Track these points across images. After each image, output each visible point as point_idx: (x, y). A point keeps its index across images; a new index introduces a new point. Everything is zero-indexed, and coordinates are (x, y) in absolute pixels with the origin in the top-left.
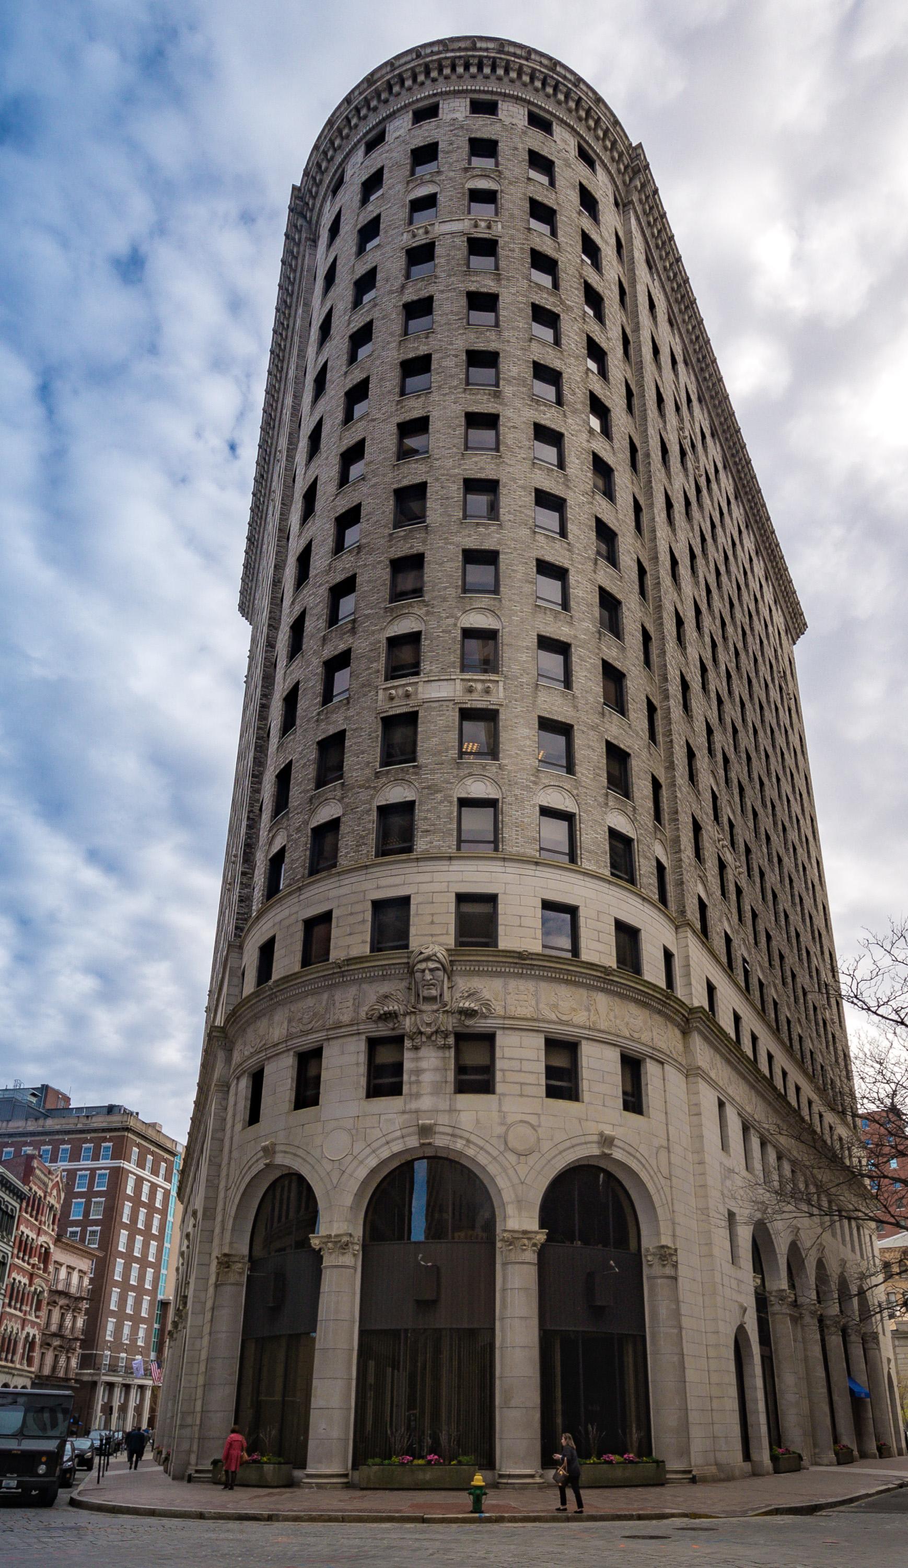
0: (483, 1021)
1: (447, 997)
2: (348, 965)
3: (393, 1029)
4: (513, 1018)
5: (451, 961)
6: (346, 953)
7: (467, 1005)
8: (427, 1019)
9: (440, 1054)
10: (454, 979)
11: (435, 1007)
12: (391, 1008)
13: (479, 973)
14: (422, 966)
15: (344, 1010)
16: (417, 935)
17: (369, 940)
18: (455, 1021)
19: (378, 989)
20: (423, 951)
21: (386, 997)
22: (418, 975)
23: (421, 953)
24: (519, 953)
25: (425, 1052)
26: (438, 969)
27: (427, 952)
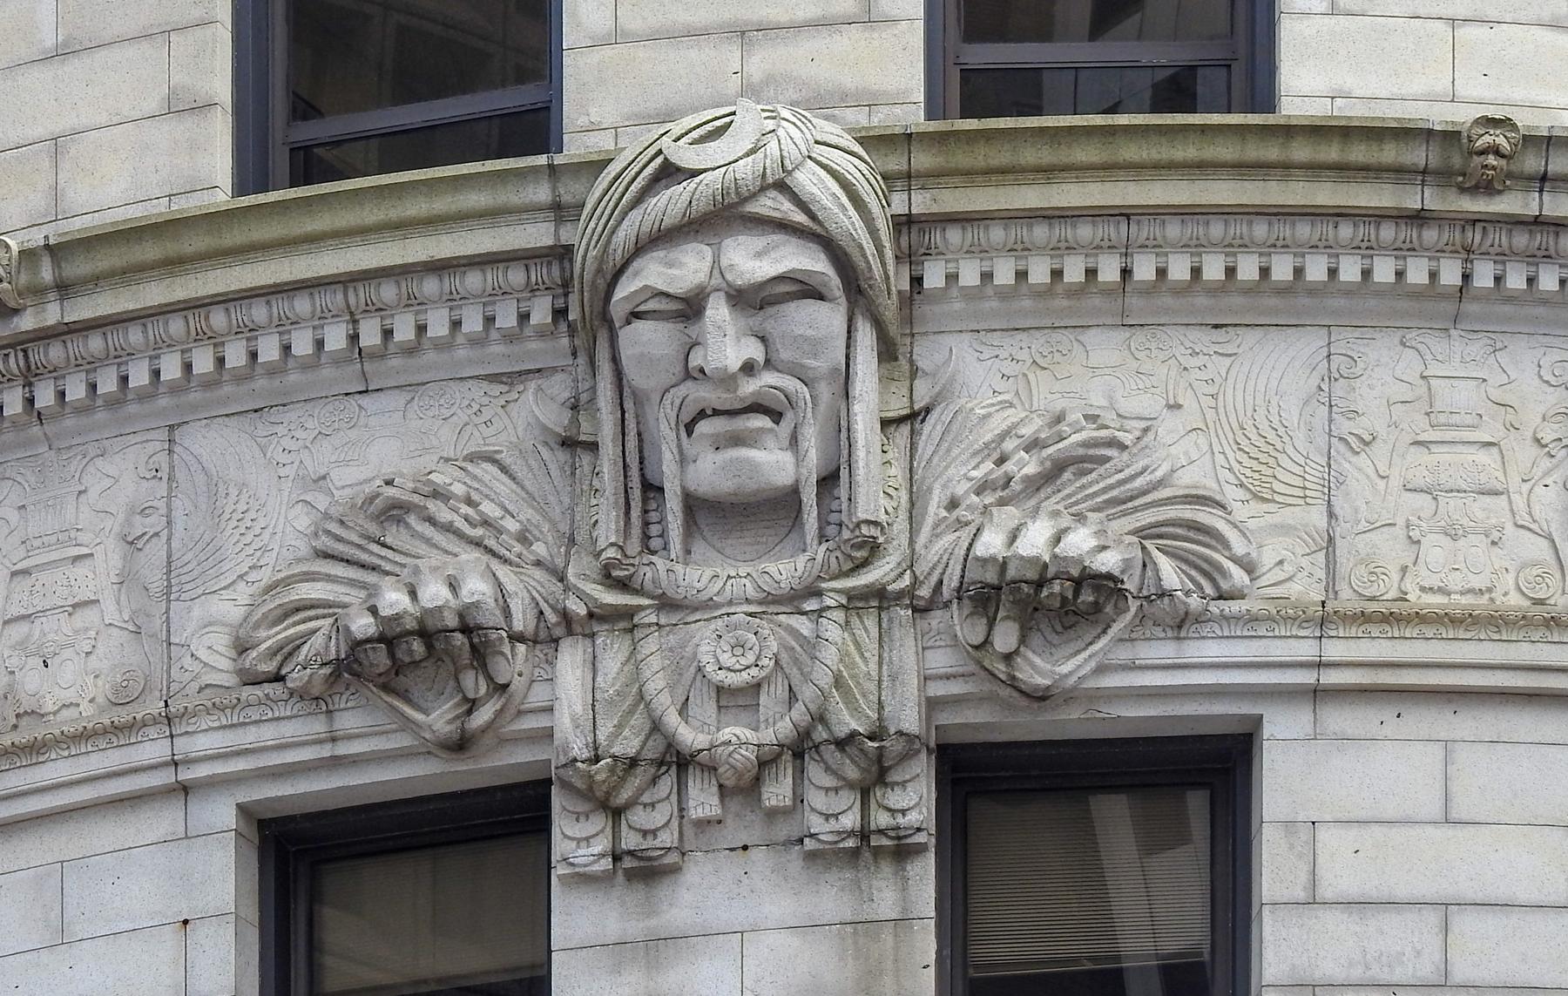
0: (1163, 651)
1: (874, 490)
2: (64, 289)
3: (460, 745)
4: (1393, 619)
5: (903, 223)
6: (35, 200)
7: (1035, 541)
8: (716, 651)
9: (830, 899)
10: (927, 354)
11: (786, 570)
12: (434, 593)
13: (1125, 305)
14: (687, 267)
15: (53, 628)
16: (617, 37)
17: (222, 88)
18: (940, 660)
19: (321, 458)
20: (685, 156)
21: (394, 512)
22: (646, 343)
23: (669, 173)
24: (1450, 137)
25: (704, 893)
26: (805, 289)
27: (722, 163)
